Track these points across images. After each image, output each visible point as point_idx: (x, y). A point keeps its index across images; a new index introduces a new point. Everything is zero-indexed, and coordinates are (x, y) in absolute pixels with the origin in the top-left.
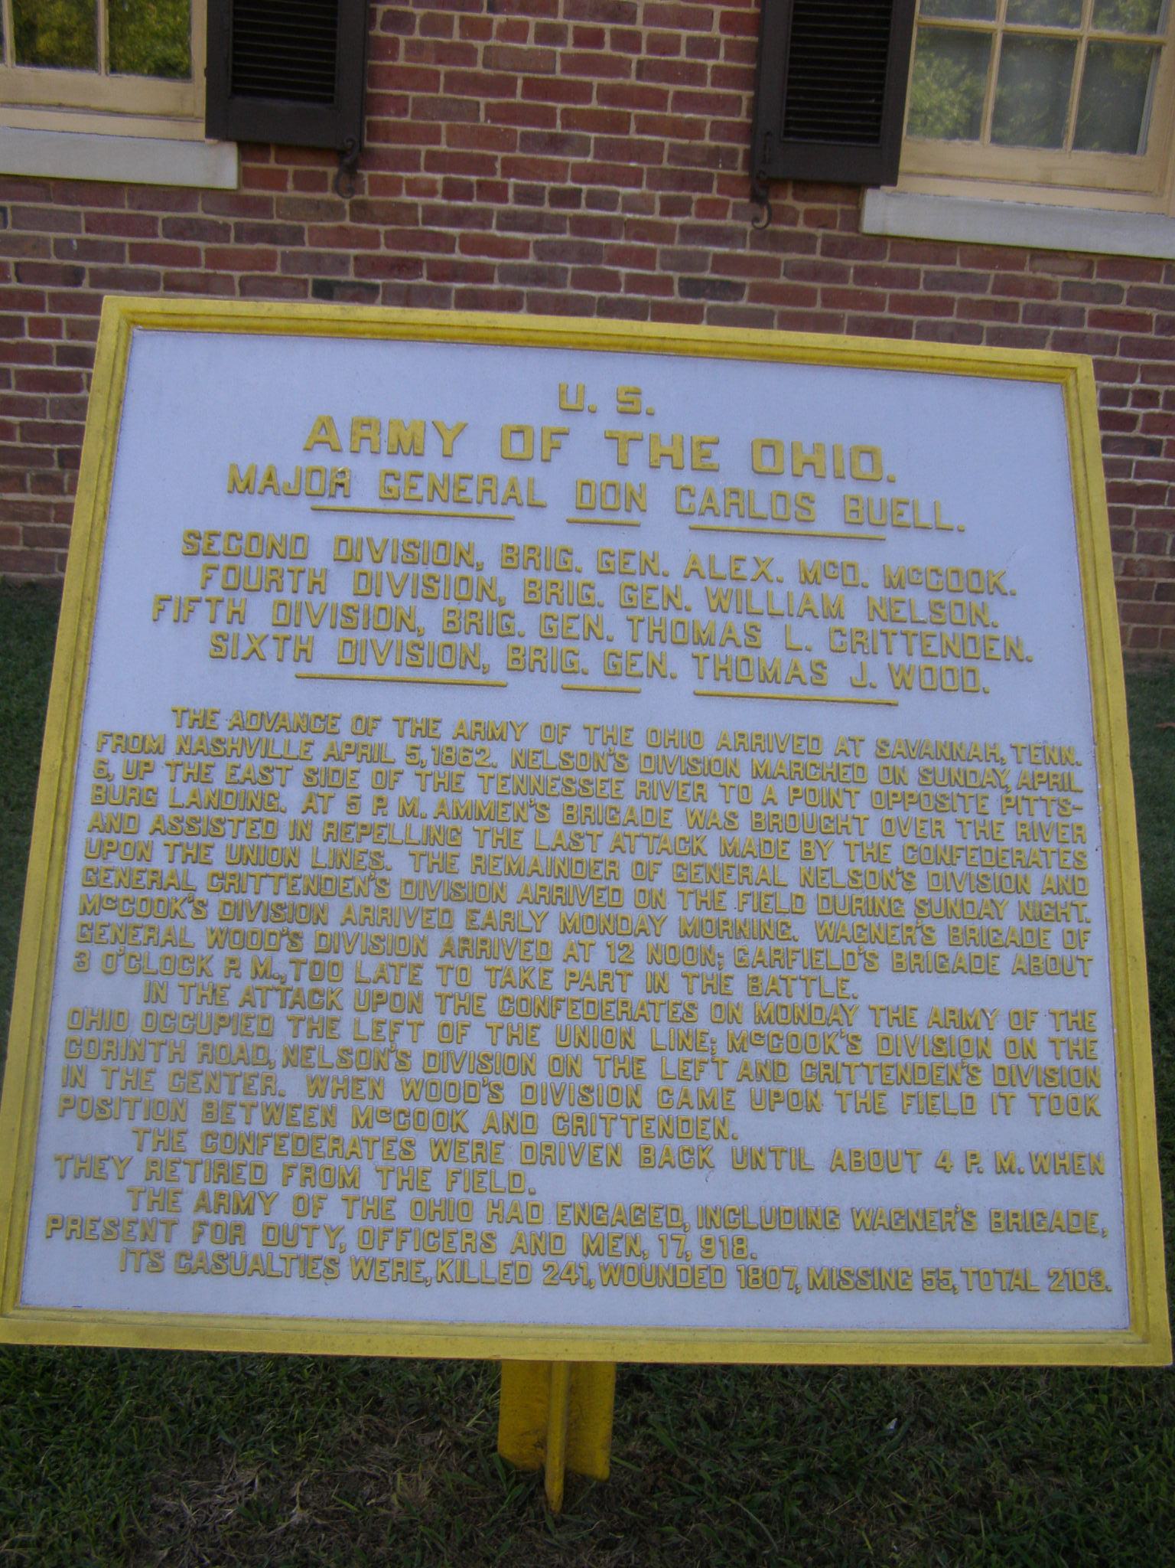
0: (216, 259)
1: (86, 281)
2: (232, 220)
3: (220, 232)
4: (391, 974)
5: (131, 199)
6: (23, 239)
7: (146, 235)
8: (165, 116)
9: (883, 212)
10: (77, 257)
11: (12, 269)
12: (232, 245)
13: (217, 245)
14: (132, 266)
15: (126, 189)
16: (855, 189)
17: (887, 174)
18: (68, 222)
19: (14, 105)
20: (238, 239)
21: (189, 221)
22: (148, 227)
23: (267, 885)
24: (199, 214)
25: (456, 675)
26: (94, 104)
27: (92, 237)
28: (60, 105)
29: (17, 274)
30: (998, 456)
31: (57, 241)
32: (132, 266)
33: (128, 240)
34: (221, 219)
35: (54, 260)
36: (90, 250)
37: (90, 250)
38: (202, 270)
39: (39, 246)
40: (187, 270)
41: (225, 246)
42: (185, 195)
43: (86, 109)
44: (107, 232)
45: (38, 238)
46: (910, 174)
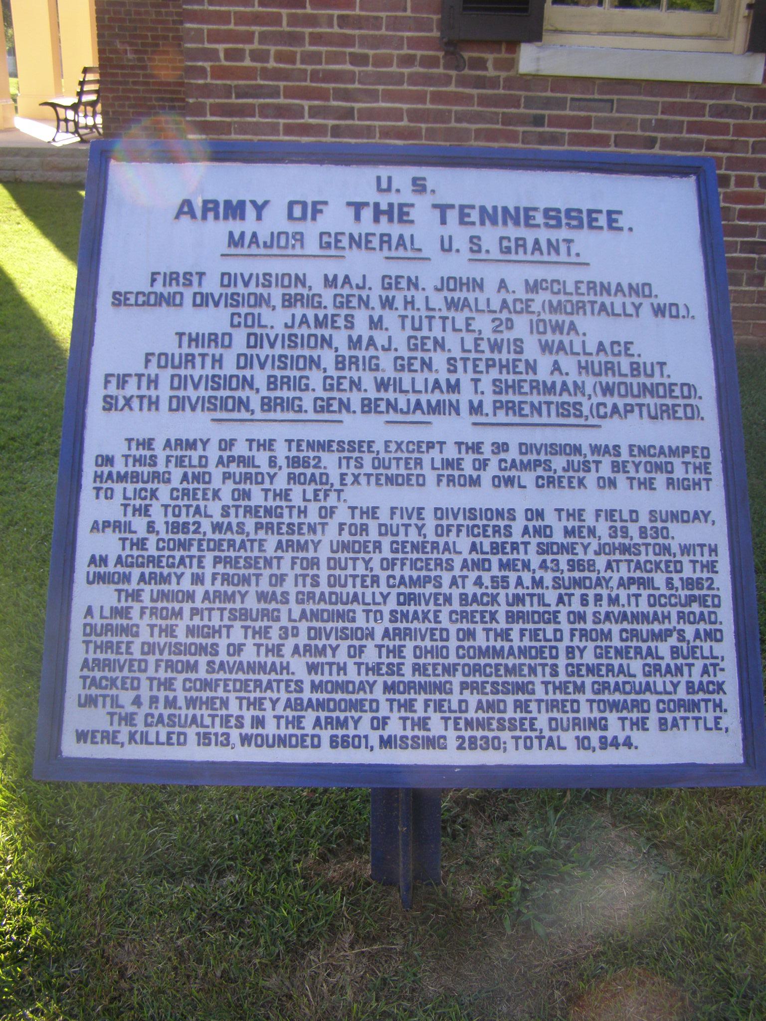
0: (740, 130)
1: (658, 145)
2: (752, 105)
3: (744, 112)
4: (670, 688)
5: (692, 92)
6: (621, 119)
7: (697, 116)
8: (699, 37)
9: (530, 59)
10: (654, 131)
11: (613, 139)
12: (751, 121)
13: (740, 121)
14: (688, 136)
15: (689, 87)
16: (513, 45)
17: (535, 35)
18: (651, 108)
19: (605, 33)
20: (755, 117)
21: (727, 106)
22: (700, 110)
23: (216, 614)
24: (733, 101)
25: (235, 415)
26: (656, 30)
27: (665, 117)
28: (634, 32)
29: (615, 142)
30: (652, 232)
31: (643, 121)
32: (688, 136)
33: (686, 119)
34: (745, 104)
35: (639, 133)
36: (662, 126)
37: (662, 126)
38: (730, 138)
39: (631, 124)
40: (721, 137)
41: (746, 121)
42: (725, 89)
43: (650, 34)
44: (675, 114)
45: (631, 119)
46: (556, 31)
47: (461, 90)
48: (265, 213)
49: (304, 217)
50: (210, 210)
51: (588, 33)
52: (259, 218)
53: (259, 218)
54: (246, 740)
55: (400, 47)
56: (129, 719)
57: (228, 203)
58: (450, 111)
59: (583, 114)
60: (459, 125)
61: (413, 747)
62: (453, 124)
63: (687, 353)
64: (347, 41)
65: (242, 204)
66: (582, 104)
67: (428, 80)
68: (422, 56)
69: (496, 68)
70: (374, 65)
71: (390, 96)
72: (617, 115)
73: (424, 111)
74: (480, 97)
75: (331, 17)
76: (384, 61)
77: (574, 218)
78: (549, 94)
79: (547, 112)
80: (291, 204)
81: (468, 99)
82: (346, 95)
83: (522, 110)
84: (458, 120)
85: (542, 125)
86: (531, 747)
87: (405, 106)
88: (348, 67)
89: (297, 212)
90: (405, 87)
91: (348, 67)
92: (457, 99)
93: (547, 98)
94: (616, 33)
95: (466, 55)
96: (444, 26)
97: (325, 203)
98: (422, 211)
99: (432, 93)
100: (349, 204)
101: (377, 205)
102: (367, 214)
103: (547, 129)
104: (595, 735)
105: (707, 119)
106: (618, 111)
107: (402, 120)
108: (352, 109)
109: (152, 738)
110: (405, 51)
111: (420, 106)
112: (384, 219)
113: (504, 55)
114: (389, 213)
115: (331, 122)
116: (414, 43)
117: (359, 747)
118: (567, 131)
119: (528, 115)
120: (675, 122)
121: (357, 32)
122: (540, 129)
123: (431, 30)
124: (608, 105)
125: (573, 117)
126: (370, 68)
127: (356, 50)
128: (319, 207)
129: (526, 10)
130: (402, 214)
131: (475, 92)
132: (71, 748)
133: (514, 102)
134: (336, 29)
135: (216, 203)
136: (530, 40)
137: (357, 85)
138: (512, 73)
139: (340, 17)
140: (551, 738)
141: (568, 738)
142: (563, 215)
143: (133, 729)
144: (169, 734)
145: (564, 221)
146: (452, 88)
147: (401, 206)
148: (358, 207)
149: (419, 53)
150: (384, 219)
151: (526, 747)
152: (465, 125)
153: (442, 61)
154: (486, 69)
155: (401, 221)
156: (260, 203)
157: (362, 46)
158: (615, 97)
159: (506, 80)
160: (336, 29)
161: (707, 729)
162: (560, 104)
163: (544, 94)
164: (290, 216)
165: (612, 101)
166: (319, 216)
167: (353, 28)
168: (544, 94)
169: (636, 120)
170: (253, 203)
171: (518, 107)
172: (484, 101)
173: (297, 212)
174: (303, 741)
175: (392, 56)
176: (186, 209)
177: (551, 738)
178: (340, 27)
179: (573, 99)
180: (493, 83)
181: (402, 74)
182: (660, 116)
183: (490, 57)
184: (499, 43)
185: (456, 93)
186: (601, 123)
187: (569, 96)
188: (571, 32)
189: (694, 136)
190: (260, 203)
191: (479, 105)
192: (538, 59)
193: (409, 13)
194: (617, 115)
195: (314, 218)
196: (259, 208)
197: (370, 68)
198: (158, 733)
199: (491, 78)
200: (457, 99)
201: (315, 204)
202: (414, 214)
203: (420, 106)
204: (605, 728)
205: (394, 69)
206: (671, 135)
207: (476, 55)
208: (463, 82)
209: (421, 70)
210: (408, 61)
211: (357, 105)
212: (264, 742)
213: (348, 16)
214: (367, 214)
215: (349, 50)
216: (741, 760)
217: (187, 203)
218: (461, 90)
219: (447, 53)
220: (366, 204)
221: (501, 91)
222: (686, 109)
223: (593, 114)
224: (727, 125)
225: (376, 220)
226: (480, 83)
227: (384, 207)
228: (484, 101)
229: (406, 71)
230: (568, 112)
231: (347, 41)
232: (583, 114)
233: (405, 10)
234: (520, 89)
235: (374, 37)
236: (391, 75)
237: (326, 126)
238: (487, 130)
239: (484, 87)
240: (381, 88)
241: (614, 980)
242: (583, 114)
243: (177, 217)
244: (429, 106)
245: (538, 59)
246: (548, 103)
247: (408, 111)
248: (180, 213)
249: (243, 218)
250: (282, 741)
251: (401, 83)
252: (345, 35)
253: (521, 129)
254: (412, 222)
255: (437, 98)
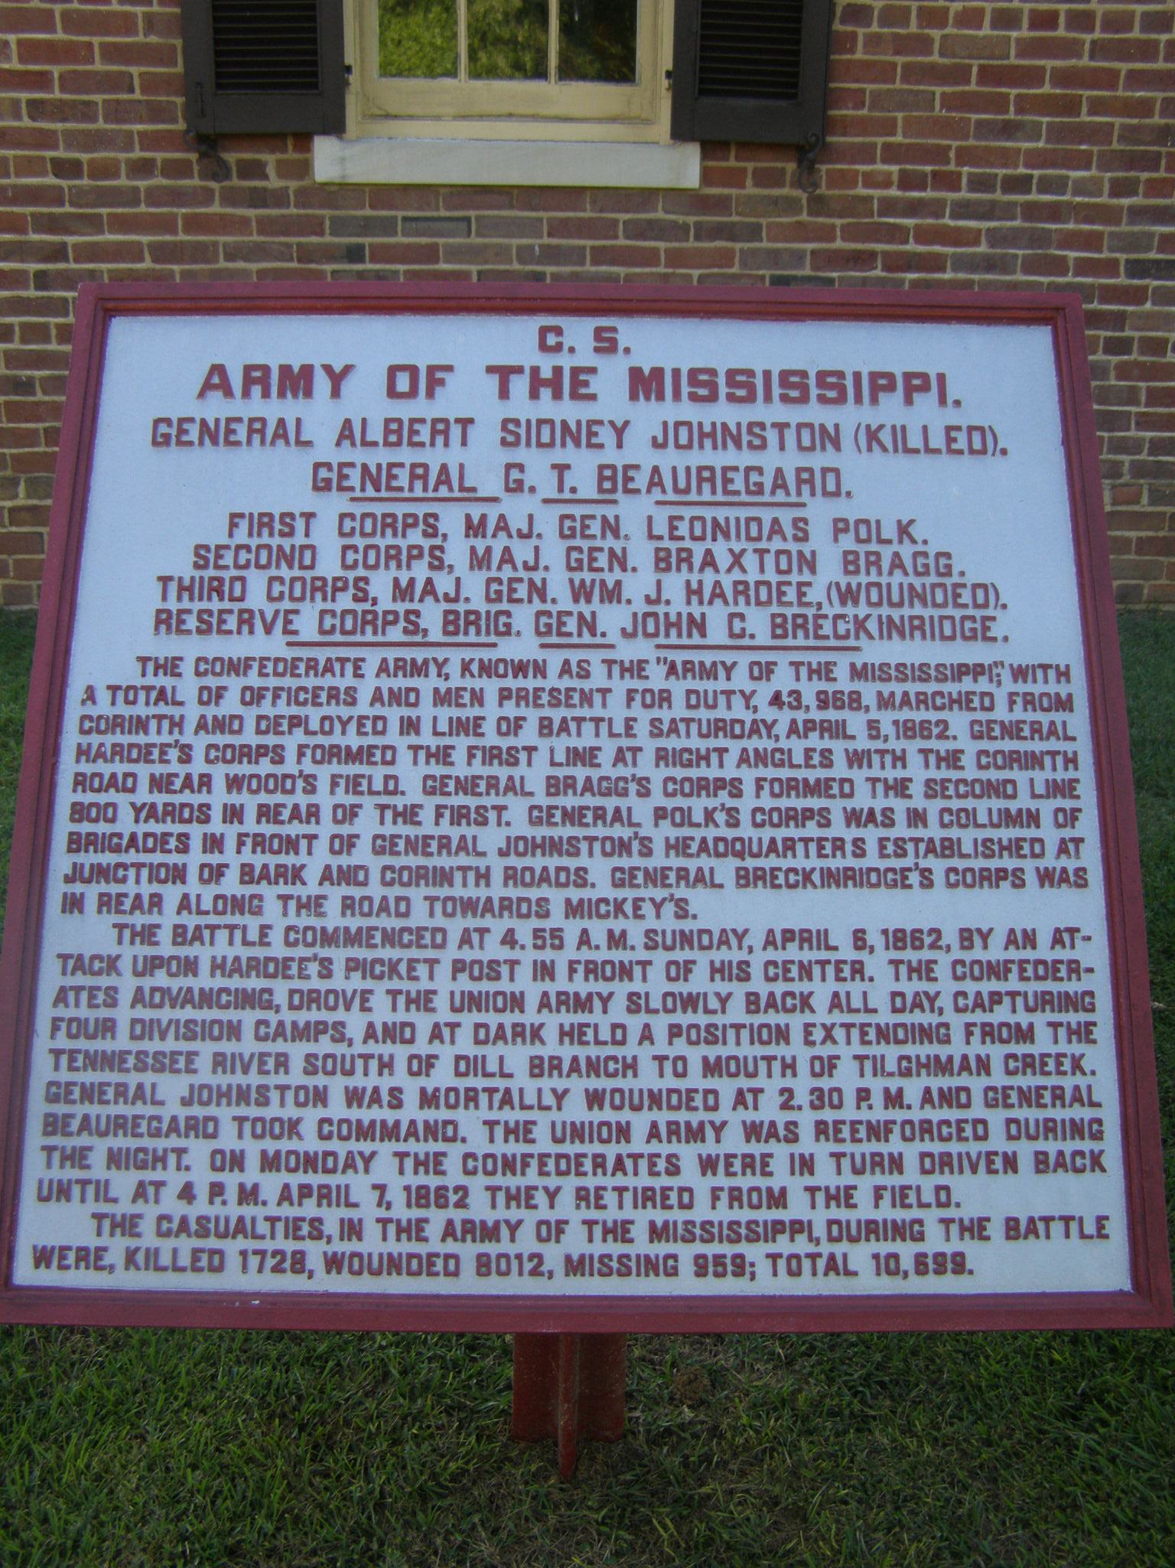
2: (691, 220)
5: (594, 202)
6: (485, 247)
8: (613, 120)
9: (329, 160)
12: (691, 243)
16: (304, 141)
17: (336, 127)
20: (697, 238)
21: (650, 222)
22: (609, 229)
24: (660, 215)
27: (554, 241)
31: (520, 248)
33: (589, 243)
34: (680, 219)
35: (516, 266)
38: (661, 270)
42: (646, 196)
43: (535, 118)
44: (570, 236)
47: (229, 210)
48: (346, 387)
49: (413, 393)
50: (256, 381)
51: (438, 118)
52: (336, 393)
53: (336, 393)
54: (333, 1263)
55: (129, 147)
56: (128, 1225)
57: (285, 370)
58: (215, 244)
59: (424, 240)
60: (231, 265)
61: (620, 1274)
62: (222, 264)
63: (1042, 617)
64: (46, 140)
65: (307, 371)
66: (422, 225)
67: (177, 197)
68: (165, 161)
69: (281, 175)
70: (92, 176)
71: (121, 224)
72: (479, 240)
73: (175, 244)
74: (261, 221)
75: (16, 103)
76: (106, 170)
77: (794, 386)
78: (368, 212)
79: (367, 241)
80: (393, 371)
81: (243, 224)
82: (53, 224)
83: (328, 239)
84: (230, 257)
85: (362, 260)
86: (799, 1273)
87: (145, 239)
88: (51, 180)
89: (403, 383)
90: (143, 209)
91: (51, 180)
92: (224, 224)
93: (366, 219)
94: (481, 117)
95: (231, 157)
96: (196, 110)
97: (449, 368)
98: (610, 380)
99: (185, 217)
100: (490, 370)
101: (535, 370)
102: (520, 385)
103: (369, 266)
104: (907, 1251)
105: (622, 242)
106: (479, 234)
107: (141, 260)
108: (64, 245)
109: (165, 1259)
110: (137, 154)
111: (168, 238)
112: (546, 393)
113: (291, 155)
114: (555, 384)
115: (33, 267)
116: (150, 141)
117: (507, 1273)
118: (402, 268)
119: (338, 246)
120: (573, 248)
121: (59, 126)
122: (359, 267)
123: (175, 121)
124: (463, 225)
125: (409, 246)
126: (85, 182)
127: (61, 153)
128: (439, 375)
129: (315, 86)
130: (576, 383)
131: (251, 213)
132: (25, 1273)
133: (315, 227)
134: (26, 122)
135: (266, 369)
136: (325, 132)
137: (68, 209)
138: (305, 183)
139: (31, 103)
140: (832, 1257)
141: (860, 1255)
142: (812, 381)
143: (133, 1243)
144: (196, 1253)
145: (814, 392)
146: (216, 208)
147: (575, 371)
148: (504, 374)
149: (159, 156)
150: (546, 393)
151: (790, 1273)
152: (240, 265)
153: (196, 168)
154: (266, 177)
155: (575, 396)
156: (338, 369)
157: (69, 147)
158: (472, 213)
159: (299, 192)
160: (26, 122)
161: (1083, 1236)
162: (387, 227)
163: (359, 213)
164: (392, 393)
165: (468, 220)
166: (438, 390)
167: (53, 120)
168: (359, 213)
169: (508, 248)
170: (328, 369)
171: (321, 234)
172: (266, 226)
173: (403, 383)
174: (431, 1264)
175: (117, 162)
176: (216, 380)
177: (832, 1257)
178: (33, 118)
179: (405, 219)
180: (279, 198)
181: (136, 189)
182: (546, 240)
183: (270, 159)
184: (281, 137)
185: (222, 216)
186: (454, 254)
187: (400, 214)
188: (411, 117)
189: (604, 268)
190: (338, 369)
191: (260, 232)
192: (343, 160)
193: (137, 95)
194: (479, 240)
195: (430, 394)
196: (337, 378)
197: (85, 182)
198: (175, 1251)
199: (274, 191)
200: (224, 224)
201: (432, 370)
202: (596, 385)
203: (168, 238)
204: (920, 1237)
205: (123, 181)
206: (566, 269)
207: (247, 156)
208: (231, 198)
209: (165, 182)
210: (142, 168)
211: (71, 240)
212: (360, 1264)
213: (42, 102)
214: (520, 385)
215: (50, 154)
216: (1126, 1285)
217: (219, 369)
218: (229, 210)
219: (203, 156)
220: (519, 370)
221: (293, 211)
222: (584, 229)
223: (441, 241)
224: (655, 252)
225: (534, 395)
226: (259, 198)
227: (546, 373)
228: (266, 226)
229: (142, 184)
230: (400, 239)
231: (46, 140)
232: (424, 240)
233: (132, 90)
234: (321, 206)
235: (86, 133)
236: (117, 191)
237: (25, 272)
238: (275, 271)
239: (265, 206)
240: (104, 211)
241: (302, 1428)
242: (424, 240)
243: (202, 395)
244: (182, 237)
245: (343, 160)
246: (367, 226)
247: (151, 245)
248: (207, 387)
249: (308, 393)
250: (394, 1264)
251: (136, 202)
252: (40, 131)
253: (329, 267)
254: (593, 397)
255: (194, 224)
